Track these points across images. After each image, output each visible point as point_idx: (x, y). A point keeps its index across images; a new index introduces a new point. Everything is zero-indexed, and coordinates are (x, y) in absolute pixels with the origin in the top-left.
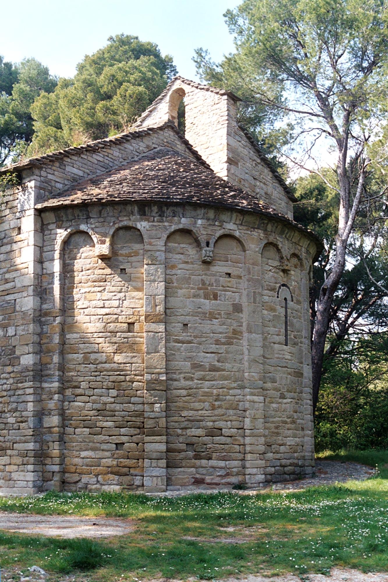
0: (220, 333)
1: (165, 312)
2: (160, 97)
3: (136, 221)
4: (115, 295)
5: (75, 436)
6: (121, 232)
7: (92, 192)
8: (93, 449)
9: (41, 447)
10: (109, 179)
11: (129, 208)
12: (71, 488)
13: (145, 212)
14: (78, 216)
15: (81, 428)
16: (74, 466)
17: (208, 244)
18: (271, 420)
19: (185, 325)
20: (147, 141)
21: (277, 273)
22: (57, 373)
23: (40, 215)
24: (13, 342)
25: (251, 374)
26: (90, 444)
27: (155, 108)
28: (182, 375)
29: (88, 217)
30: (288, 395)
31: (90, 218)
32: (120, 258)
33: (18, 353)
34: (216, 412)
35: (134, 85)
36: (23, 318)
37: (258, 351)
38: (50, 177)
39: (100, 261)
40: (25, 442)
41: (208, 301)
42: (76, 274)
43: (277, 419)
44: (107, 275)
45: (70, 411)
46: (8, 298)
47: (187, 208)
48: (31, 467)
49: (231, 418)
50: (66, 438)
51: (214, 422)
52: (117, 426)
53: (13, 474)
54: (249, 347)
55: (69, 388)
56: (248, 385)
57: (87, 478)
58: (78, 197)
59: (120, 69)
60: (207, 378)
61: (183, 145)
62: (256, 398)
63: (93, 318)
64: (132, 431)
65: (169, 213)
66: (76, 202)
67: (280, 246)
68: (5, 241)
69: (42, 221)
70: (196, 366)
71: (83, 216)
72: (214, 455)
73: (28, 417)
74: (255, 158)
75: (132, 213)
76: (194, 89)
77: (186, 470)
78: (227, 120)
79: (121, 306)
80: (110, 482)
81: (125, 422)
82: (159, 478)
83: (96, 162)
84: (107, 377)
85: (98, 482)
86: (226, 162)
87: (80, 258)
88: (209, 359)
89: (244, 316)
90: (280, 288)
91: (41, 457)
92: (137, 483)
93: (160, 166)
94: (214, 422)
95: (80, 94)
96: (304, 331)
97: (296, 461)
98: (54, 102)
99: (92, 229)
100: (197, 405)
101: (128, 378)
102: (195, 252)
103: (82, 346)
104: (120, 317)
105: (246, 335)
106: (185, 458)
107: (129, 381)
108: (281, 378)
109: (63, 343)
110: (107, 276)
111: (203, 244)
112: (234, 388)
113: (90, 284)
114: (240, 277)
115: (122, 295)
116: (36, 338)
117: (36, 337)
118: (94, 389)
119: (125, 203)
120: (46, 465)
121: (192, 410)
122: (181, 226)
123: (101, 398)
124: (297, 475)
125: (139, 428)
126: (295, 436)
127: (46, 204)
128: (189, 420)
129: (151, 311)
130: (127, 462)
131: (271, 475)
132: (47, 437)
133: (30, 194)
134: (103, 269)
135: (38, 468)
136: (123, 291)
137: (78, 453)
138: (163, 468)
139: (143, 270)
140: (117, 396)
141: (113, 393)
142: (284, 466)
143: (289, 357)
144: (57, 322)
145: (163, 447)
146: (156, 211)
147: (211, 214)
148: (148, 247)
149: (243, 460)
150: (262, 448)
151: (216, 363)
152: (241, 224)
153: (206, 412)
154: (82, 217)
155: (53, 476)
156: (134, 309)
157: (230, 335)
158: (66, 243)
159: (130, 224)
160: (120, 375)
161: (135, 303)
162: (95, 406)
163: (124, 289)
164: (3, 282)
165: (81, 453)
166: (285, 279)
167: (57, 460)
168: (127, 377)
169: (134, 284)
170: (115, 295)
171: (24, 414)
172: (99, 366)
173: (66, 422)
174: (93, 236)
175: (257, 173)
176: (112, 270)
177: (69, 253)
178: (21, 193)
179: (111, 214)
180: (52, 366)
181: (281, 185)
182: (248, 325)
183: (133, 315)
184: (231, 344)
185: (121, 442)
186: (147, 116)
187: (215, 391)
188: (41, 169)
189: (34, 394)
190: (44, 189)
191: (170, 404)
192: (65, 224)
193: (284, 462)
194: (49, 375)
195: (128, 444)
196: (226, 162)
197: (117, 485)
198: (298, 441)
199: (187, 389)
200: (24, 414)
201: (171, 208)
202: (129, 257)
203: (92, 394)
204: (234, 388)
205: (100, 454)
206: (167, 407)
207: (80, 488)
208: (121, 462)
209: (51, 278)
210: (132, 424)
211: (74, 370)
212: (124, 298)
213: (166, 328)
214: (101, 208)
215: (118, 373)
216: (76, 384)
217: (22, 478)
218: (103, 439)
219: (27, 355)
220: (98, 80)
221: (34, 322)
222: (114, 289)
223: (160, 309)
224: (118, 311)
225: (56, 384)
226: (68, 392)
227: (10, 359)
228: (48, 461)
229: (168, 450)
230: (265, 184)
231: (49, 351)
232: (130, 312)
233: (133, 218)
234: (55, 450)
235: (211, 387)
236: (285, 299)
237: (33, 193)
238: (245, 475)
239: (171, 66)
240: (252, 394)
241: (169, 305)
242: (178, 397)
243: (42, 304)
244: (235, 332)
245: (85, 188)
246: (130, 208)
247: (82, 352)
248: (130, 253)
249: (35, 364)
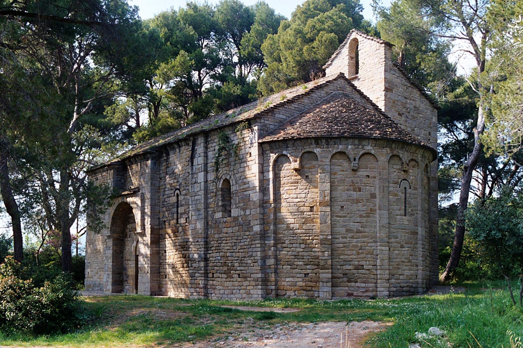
0: (363, 211)
1: (331, 200)
2: (343, 44)
3: (313, 148)
6: (306, 155)
7: (289, 132)
8: (292, 277)
9: (265, 276)
10: (300, 121)
11: (309, 141)
17: (355, 160)
18: (394, 260)
19: (342, 207)
20: (326, 89)
21: (400, 173)
22: (273, 235)
23: (261, 146)
24: (249, 218)
25: (382, 234)
26: (291, 274)
27: (340, 52)
28: (341, 236)
29: (287, 147)
30: (405, 245)
32: (306, 170)
33: (252, 224)
34: (360, 256)
35: (328, 32)
36: (254, 205)
37: (385, 221)
38: (266, 122)
39: (294, 172)
40: (257, 273)
41: (355, 193)
42: (281, 179)
43: (398, 260)
46: (246, 193)
47: (342, 139)
48: (260, 287)
49: (369, 259)
50: (278, 271)
51: (359, 261)
53: (251, 291)
54: (380, 218)
55: (279, 244)
56: (378, 241)
58: (281, 135)
59: (318, 20)
60: (355, 237)
61: (351, 87)
62: (383, 248)
63: (291, 204)
64: (313, 267)
66: (280, 139)
67: (401, 156)
68: (243, 160)
69: (263, 149)
70: (348, 231)
72: (359, 280)
74: (406, 83)
75: (311, 144)
76: (364, 38)
77: (343, 288)
78: (385, 61)
83: (294, 108)
85: (295, 295)
86: (384, 91)
88: (355, 226)
89: (377, 200)
90: (401, 181)
91: (265, 281)
92: (316, 295)
93: (331, 109)
94: (359, 261)
95: (292, 39)
96: (419, 206)
97: (411, 285)
98: (277, 41)
99: (290, 154)
100: (349, 252)
102: (348, 164)
105: (378, 211)
106: (342, 282)
108: (401, 236)
109: (276, 218)
111: (352, 160)
112: (371, 242)
113: (289, 184)
114: (375, 177)
116: (261, 216)
117: (261, 215)
119: (307, 138)
120: (268, 286)
121: (346, 255)
122: (339, 150)
124: (412, 292)
125: (317, 265)
126: (410, 270)
127: (264, 140)
128: (344, 261)
131: (393, 292)
133: (255, 134)
135: (264, 287)
139: (318, 176)
141: (303, 246)
142: (402, 287)
143: (407, 223)
145: (330, 276)
147: (356, 142)
148: (320, 163)
149: (376, 283)
150: (387, 277)
151: (360, 228)
152: (375, 146)
157: (369, 212)
158: (276, 161)
161: (314, 195)
162: (293, 253)
163: (308, 187)
164: (243, 184)
166: (405, 176)
167: (273, 283)
169: (313, 184)
171: (256, 258)
173: (278, 262)
175: (408, 94)
178: (250, 133)
179: (300, 145)
180: (270, 231)
181: (427, 99)
182: (379, 205)
184: (369, 217)
186: (335, 58)
187: (359, 244)
188: (260, 118)
189: (261, 247)
190: (263, 130)
191: (334, 252)
192: (275, 151)
193: (402, 285)
196: (384, 91)
198: (415, 271)
200: (256, 258)
201: (333, 140)
204: (371, 242)
205: (296, 279)
206: (332, 253)
211: (282, 234)
213: (331, 209)
217: (255, 293)
220: (304, 29)
221: (260, 207)
223: (328, 198)
225: (272, 242)
226: (279, 246)
227: (248, 228)
228: (269, 283)
229: (333, 278)
230: (414, 100)
231: (268, 223)
232: (311, 200)
233: (312, 146)
234: (272, 277)
235: (357, 242)
236: (405, 188)
237: (257, 133)
238: (377, 291)
239: (359, 5)
240: (381, 246)
241: (333, 196)
243: (264, 196)
244: (371, 210)
245: (286, 128)
249: (261, 231)
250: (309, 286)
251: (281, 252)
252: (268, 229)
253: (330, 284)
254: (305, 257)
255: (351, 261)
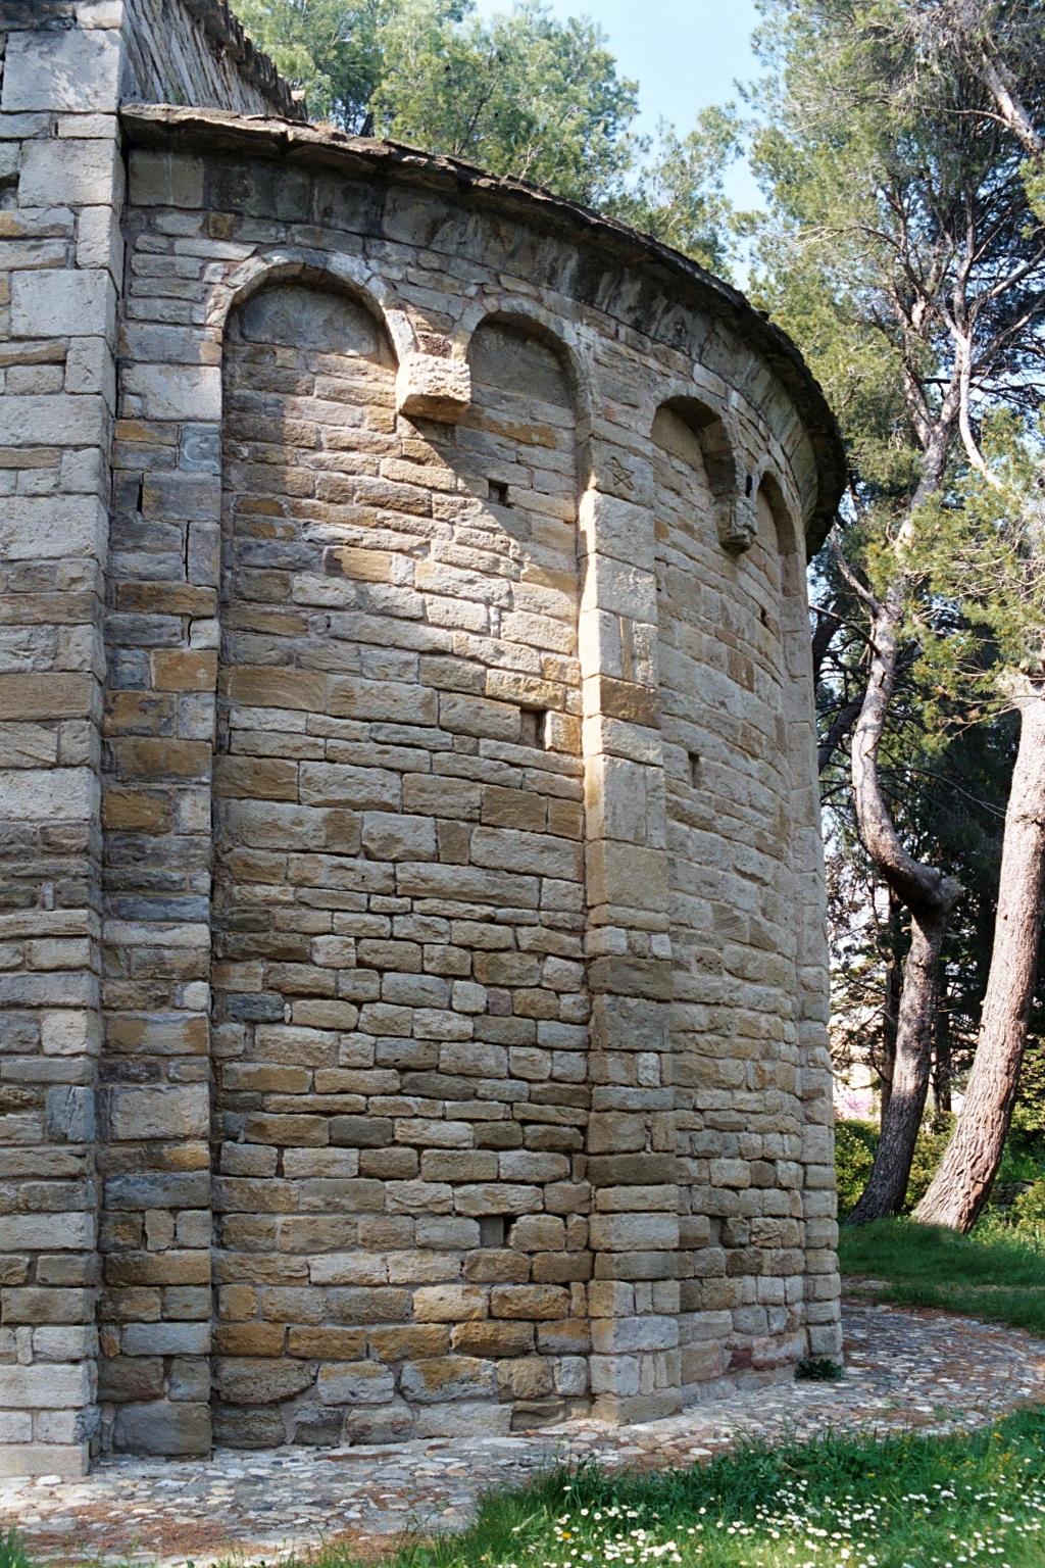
4: (471, 582)
5: (279, 1182)
12: (256, 1427)
13: (593, 290)
14: (327, 212)
15: (314, 1144)
16: (276, 1321)
26: (365, 1222)
31: (383, 238)
44: (433, 489)
45: (251, 1067)
52: (488, 1138)
55: (246, 956)
57: (348, 1379)
65: (666, 327)
71: (348, 220)
73: (46, 1084)
75: (551, 278)
79: (494, 628)
80: (457, 1390)
81: (517, 1126)
82: (662, 1357)
84: (442, 925)
85: (400, 1391)
87: (308, 393)
92: (567, 1384)
101: (526, 937)
103: (319, 770)
104: (489, 671)
107: (529, 952)
110: (436, 497)
115: (497, 586)
118: (381, 970)
120: (121, 1321)
123: (419, 1014)
125: (568, 1152)
129: (618, 673)
130: (528, 1296)
132: (140, 1187)
134: (420, 462)
136: (501, 570)
137: (297, 1261)
138: (670, 1315)
140: (487, 1011)
141: (472, 995)
144: (197, 643)
146: (630, 301)
153: (747, 1096)
154: (341, 225)
155: (167, 1374)
156: (544, 656)
159: (542, 315)
160: (491, 920)
162: (388, 1048)
165: (316, 1261)
168: (523, 931)
170: (471, 582)
172: (407, 872)
174: (393, 319)
176: (457, 476)
177: (251, 359)
179: (472, 251)
180: (172, 842)
183: (541, 675)
185: (506, 1209)
194: (152, 886)
195: (533, 1219)
197: (486, 1398)
199: (708, 1004)
202: (520, 442)
203: (373, 994)
205: (404, 1265)
207: (302, 1425)
208: (504, 1298)
209: (170, 439)
210: (545, 1135)
211: (271, 875)
212: (504, 602)
214: (443, 210)
215: (488, 910)
216: (293, 941)
218: (425, 1198)
219: (47, 774)
222: (465, 554)
224: (483, 647)
231: (151, 771)
232: (531, 661)
233: (550, 297)
234: (183, 1248)
242: (685, 1031)
246: (554, 254)
247: (319, 798)
248: (525, 429)
250: (515, 1318)
251: (264, 1032)
252: (149, 813)
253: (669, 1294)
254: (484, 1086)
255: (738, 1128)
